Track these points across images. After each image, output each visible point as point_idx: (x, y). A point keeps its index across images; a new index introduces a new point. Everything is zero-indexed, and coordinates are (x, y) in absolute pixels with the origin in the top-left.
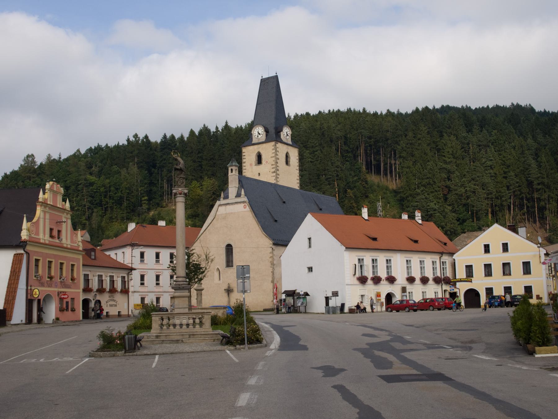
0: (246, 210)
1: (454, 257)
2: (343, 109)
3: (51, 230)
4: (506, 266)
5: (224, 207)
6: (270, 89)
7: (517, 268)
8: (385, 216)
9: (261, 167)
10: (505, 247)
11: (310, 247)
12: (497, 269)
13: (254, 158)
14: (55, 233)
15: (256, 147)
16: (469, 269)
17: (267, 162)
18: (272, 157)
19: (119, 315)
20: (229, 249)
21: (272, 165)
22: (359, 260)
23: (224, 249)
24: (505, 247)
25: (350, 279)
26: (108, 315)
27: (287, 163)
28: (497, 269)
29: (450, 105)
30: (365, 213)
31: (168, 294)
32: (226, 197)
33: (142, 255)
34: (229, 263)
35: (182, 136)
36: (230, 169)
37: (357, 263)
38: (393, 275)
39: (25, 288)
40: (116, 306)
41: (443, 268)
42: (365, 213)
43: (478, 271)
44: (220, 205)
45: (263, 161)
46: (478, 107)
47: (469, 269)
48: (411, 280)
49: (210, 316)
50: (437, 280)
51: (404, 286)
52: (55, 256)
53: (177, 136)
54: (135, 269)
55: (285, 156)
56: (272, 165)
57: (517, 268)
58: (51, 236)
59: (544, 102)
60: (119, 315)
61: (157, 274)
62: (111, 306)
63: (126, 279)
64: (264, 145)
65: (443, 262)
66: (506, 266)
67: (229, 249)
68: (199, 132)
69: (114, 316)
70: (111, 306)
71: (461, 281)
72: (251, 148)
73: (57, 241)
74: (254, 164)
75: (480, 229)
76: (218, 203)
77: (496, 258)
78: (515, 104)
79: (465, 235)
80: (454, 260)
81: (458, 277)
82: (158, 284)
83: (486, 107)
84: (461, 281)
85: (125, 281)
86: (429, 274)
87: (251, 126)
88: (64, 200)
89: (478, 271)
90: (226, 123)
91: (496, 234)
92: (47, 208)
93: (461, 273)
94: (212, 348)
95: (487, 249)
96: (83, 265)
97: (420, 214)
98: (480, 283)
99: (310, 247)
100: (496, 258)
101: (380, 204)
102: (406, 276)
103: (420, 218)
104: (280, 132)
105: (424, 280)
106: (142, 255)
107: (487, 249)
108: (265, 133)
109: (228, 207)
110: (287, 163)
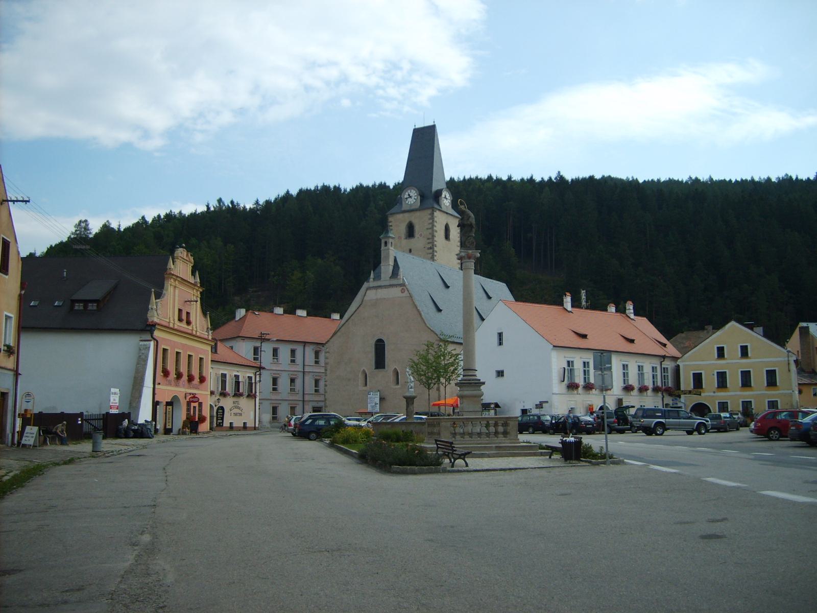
0: (404, 295)
1: (678, 363)
2: (484, 176)
3: (180, 311)
4: (746, 377)
5: (374, 291)
6: (424, 142)
7: (759, 379)
8: (587, 308)
9: (412, 240)
10: (744, 351)
11: (500, 344)
12: (734, 380)
13: (403, 228)
14: (184, 316)
15: (406, 215)
16: (698, 378)
17: (421, 235)
18: (427, 229)
19: (245, 427)
20: (380, 347)
21: (428, 239)
22: (568, 362)
23: (374, 346)
24: (744, 351)
25: (558, 387)
26: (231, 427)
27: (447, 237)
28: (734, 380)
29: (612, 176)
30: (568, 300)
31: (269, 402)
32: (378, 277)
33: (275, 351)
34: (380, 363)
35: (550, 178)
36: (383, 241)
37: (565, 366)
38: (630, 383)
39: (152, 386)
40: (241, 415)
41: (664, 376)
42: (568, 300)
43: (711, 381)
44: (369, 288)
45: (417, 234)
46: (647, 180)
47: (698, 378)
48: (628, 388)
49: (517, 422)
50: (656, 390)
51: (620, 397)
52: (184, 346)
53: (546, 179)
54: (264, 368)
55: (444, 228)
56: (428, 239)
57: (759, 379)
58: (180, 320)
59: (804, 172)
60: (245, 427)
61: (274, 376)
62: (236, 414)
63: (253, 381)
64: (418, 214)
65: (664, 368)
66: (746, 377)
67: (380, 347)
68: (394, 187)
69: (239, 429)
70: (236, 414)
71: (685, 393)
72: (400, 216)
73: (186, 326)
74: (403, 236)
75: (718, 326)
76: (366, 285)
77: (733, 365)
78: (694, 178)
79: (683, 335)
80: (678, 366)
81: (682, 388)
82: (274, 389)
83: (656, 180)
84: (685, 393)
85: (252, 383)
86: (648, 383)
87: (399, 188)
88: (193, 273)
89: (711, 381)
90: (288, 190)
91: (734, 333)
92: (177, 282)
93: (687, 382)
94: (564, 465)
95: (721, 352)
96: (212, 361)
97: (631, 307)
98: (710, 395)
99: (500, 344)
100: (733, 365)
101: (583, 293)
102: (623, 385)
103: (632, 311)
104: (439, 197)
105: (643, 389)
106: (275, 351)
107: (721, 352)
108: (419, 197)
109: (379, 290)
110: (447, 237)
